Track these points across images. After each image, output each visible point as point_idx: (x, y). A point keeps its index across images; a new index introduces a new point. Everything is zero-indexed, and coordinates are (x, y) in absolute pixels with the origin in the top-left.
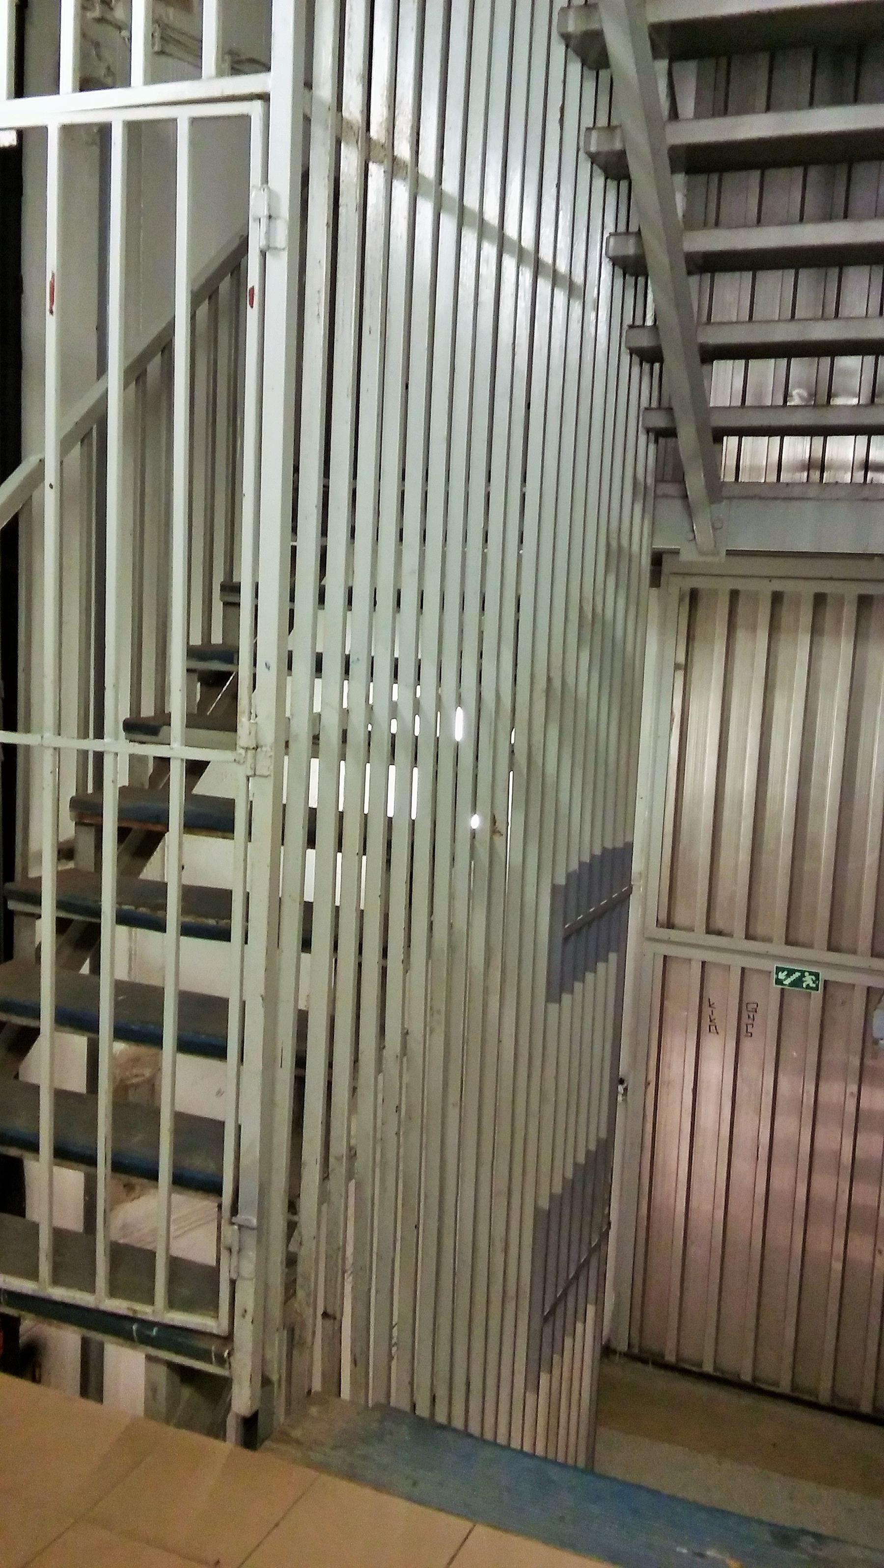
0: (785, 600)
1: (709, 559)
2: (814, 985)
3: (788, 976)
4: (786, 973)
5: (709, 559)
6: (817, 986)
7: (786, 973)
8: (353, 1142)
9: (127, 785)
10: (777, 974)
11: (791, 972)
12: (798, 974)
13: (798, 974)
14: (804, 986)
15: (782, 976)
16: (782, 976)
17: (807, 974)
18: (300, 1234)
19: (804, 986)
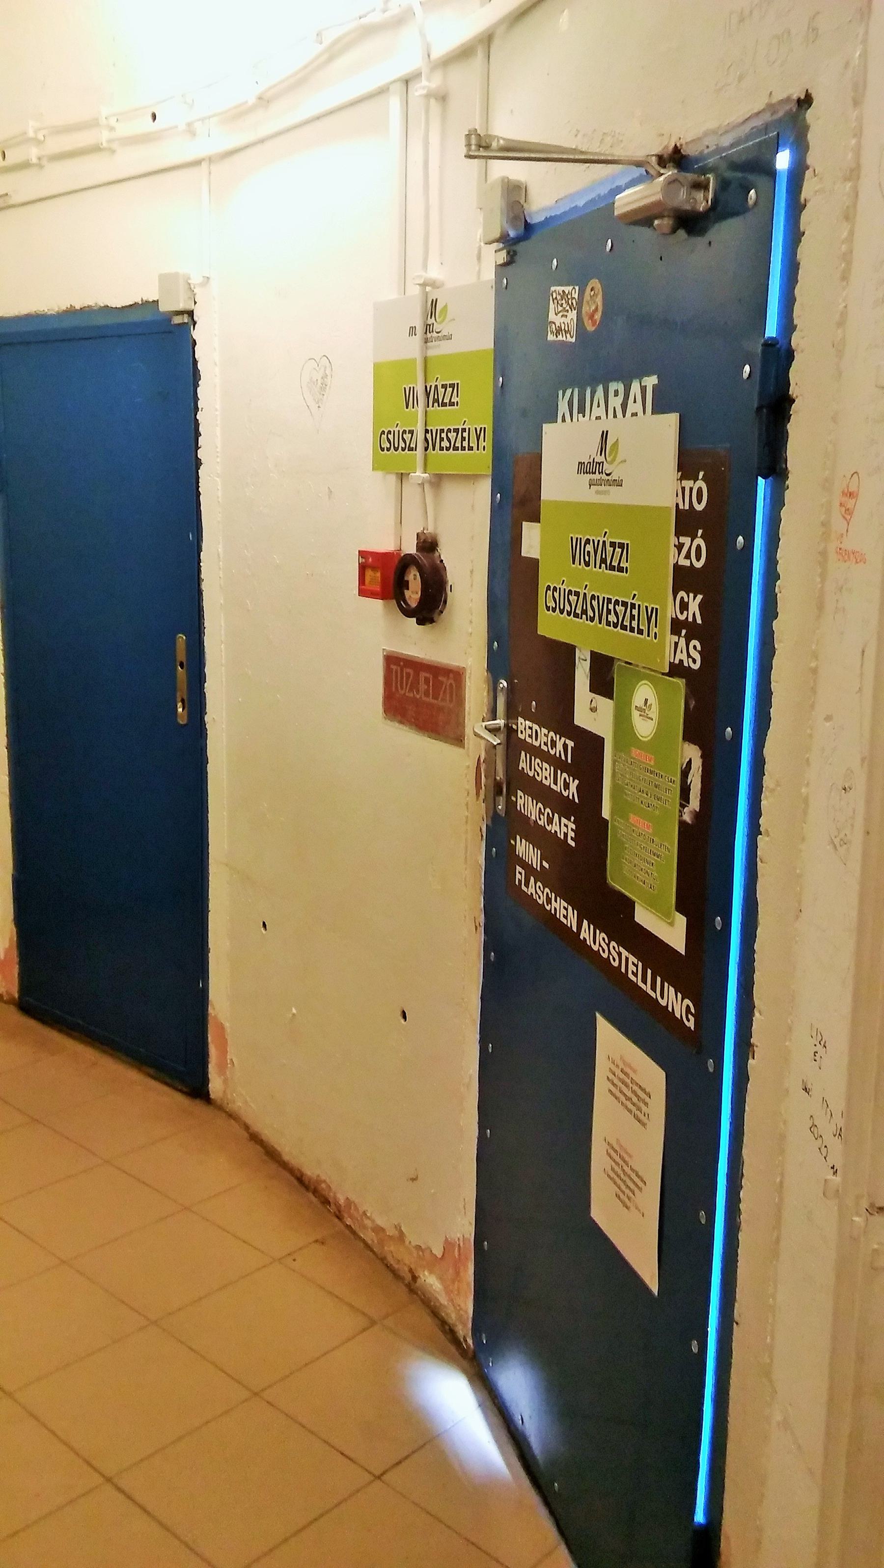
18: (215, 1017)
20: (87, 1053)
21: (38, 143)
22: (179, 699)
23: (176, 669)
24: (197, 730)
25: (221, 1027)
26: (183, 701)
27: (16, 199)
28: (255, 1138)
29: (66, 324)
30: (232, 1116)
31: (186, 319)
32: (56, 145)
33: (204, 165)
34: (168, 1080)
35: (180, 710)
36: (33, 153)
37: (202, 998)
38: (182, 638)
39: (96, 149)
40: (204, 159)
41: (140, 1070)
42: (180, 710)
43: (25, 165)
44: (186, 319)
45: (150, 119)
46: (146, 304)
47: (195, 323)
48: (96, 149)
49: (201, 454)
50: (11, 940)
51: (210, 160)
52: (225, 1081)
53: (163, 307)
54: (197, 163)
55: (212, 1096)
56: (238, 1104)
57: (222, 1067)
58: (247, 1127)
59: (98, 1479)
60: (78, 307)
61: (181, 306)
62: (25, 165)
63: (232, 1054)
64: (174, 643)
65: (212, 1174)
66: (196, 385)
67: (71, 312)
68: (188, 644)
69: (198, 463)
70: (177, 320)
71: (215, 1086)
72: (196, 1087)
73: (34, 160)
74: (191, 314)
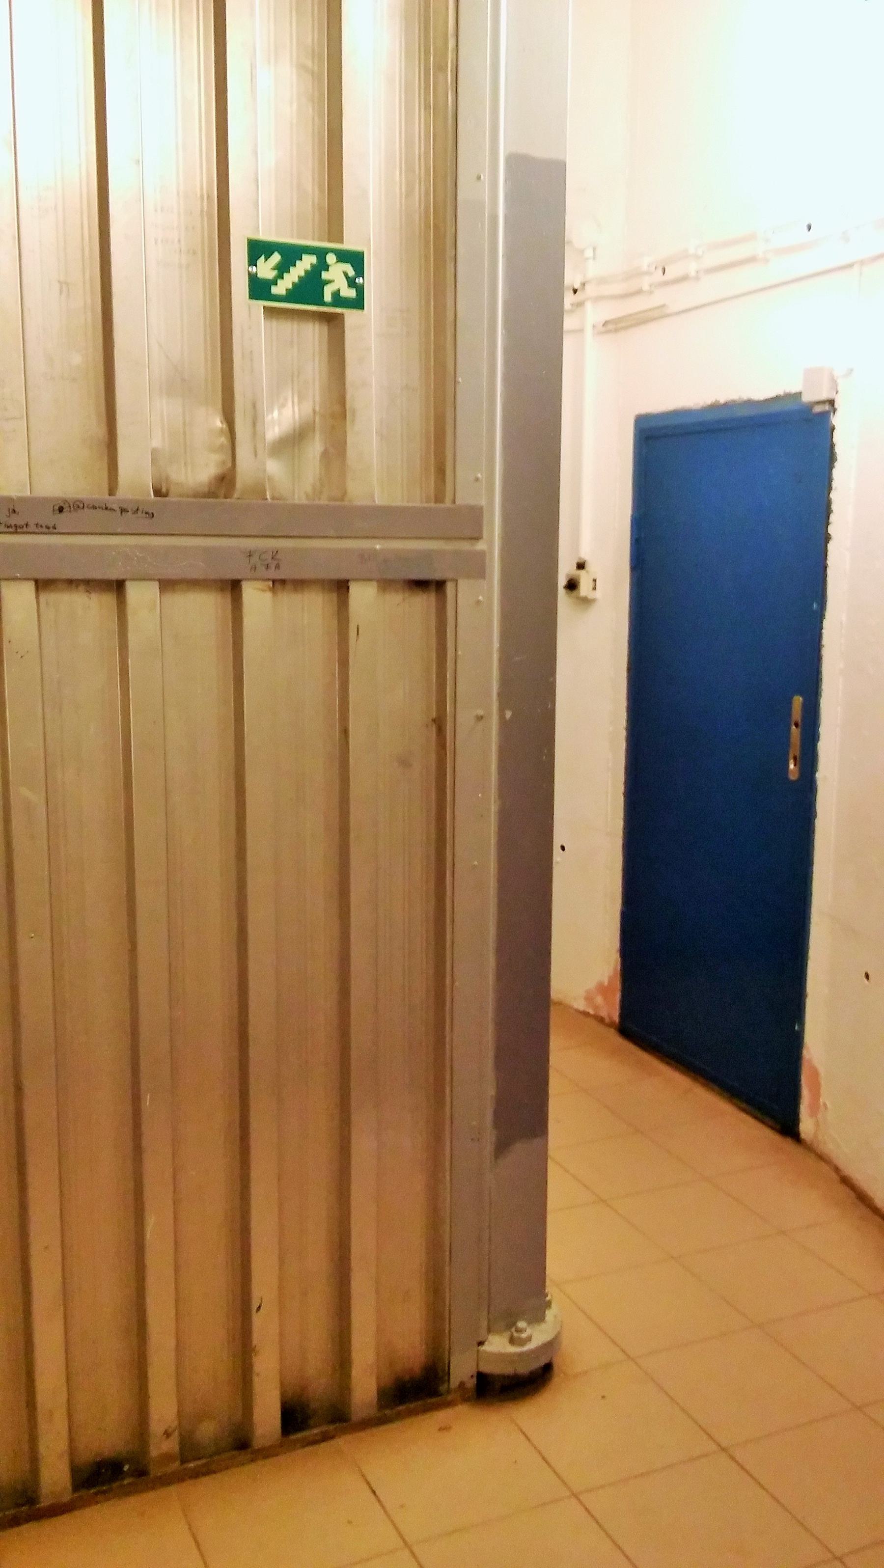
0: (523, 150)
1: (338, 503)
2: (352, 293)
3: (282, 269)
4: (276, 258)
5: (338, 503)
6: (360, 290)
7: (276, 258)
8: (607, 1020)
9: (606, 984)
10: (253, 262)
11: (290, 255)
12: (307, 262)
13: (307, 262)
14: (328, 298)
15: (266, 269)
16: (266, 269)
17: (331, 258)
18: (809, 1061)
19: (328, 298)
20: (680, 1080)
21: (697, 257)
22: (791, 756)
23: (789, 729)
24: (806, 788)
25: (815, 1074)
26: (795, 758)
27: (673, 308)
28: (846, 1181)
29: (709, 417)
30: (821, 1157)
31: (827, 407)
32: (711, 260)
33: (856, 268)
34: (759, 1115)
35: (792, 766)
36: (692, 268)
37: (795, 1042)
38: (798, 701)
39: (752, 260)
40: (856, 262)
41: (731, 1102)
42: (792, 766)
43: (684, 278)
44: (827, 407)
45: (806, 228)
46: (788, 396)
47: (835, 411)
48: (752, 260)
49: (831, 530)
50: (615, 969)
51: (862, 263)
52: (817, 1124)
53: (807, 398)
54: (850, 266)
55: (803, 1135)
56: (829, 1147)
57: (815, 1108)
58: (837, 1170)
59: (714, 1447)
60: (722, 401)
61: (824, 396)
62: (684, 278)
63: (825, 1098)
64: (790, 703)
65: (804, 1206)
66: (831, 467)
67: (715, 407)
68: (804, 706)
69: (827, 538)
70: (818, 409)
71: (806, 1126)
72: (786, 1124)
73: (693, 274)
74: (832, 402)
